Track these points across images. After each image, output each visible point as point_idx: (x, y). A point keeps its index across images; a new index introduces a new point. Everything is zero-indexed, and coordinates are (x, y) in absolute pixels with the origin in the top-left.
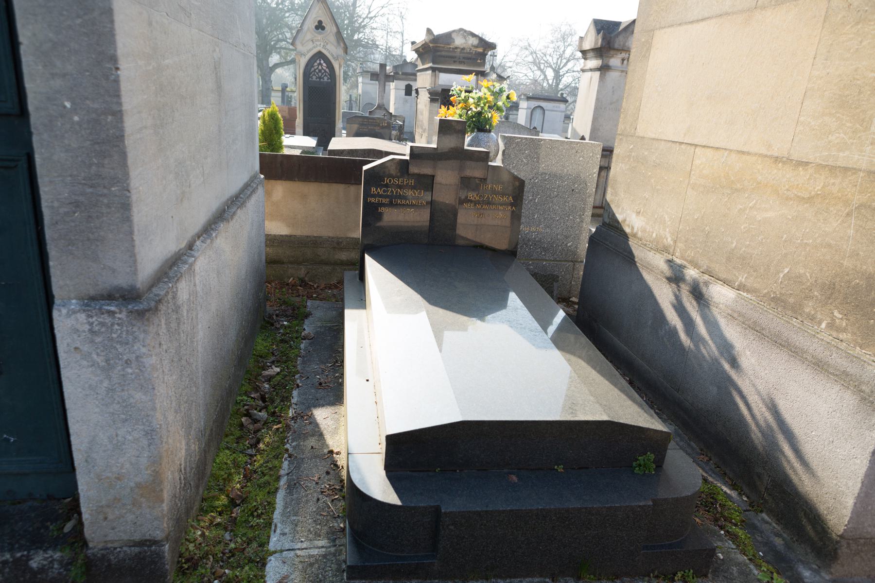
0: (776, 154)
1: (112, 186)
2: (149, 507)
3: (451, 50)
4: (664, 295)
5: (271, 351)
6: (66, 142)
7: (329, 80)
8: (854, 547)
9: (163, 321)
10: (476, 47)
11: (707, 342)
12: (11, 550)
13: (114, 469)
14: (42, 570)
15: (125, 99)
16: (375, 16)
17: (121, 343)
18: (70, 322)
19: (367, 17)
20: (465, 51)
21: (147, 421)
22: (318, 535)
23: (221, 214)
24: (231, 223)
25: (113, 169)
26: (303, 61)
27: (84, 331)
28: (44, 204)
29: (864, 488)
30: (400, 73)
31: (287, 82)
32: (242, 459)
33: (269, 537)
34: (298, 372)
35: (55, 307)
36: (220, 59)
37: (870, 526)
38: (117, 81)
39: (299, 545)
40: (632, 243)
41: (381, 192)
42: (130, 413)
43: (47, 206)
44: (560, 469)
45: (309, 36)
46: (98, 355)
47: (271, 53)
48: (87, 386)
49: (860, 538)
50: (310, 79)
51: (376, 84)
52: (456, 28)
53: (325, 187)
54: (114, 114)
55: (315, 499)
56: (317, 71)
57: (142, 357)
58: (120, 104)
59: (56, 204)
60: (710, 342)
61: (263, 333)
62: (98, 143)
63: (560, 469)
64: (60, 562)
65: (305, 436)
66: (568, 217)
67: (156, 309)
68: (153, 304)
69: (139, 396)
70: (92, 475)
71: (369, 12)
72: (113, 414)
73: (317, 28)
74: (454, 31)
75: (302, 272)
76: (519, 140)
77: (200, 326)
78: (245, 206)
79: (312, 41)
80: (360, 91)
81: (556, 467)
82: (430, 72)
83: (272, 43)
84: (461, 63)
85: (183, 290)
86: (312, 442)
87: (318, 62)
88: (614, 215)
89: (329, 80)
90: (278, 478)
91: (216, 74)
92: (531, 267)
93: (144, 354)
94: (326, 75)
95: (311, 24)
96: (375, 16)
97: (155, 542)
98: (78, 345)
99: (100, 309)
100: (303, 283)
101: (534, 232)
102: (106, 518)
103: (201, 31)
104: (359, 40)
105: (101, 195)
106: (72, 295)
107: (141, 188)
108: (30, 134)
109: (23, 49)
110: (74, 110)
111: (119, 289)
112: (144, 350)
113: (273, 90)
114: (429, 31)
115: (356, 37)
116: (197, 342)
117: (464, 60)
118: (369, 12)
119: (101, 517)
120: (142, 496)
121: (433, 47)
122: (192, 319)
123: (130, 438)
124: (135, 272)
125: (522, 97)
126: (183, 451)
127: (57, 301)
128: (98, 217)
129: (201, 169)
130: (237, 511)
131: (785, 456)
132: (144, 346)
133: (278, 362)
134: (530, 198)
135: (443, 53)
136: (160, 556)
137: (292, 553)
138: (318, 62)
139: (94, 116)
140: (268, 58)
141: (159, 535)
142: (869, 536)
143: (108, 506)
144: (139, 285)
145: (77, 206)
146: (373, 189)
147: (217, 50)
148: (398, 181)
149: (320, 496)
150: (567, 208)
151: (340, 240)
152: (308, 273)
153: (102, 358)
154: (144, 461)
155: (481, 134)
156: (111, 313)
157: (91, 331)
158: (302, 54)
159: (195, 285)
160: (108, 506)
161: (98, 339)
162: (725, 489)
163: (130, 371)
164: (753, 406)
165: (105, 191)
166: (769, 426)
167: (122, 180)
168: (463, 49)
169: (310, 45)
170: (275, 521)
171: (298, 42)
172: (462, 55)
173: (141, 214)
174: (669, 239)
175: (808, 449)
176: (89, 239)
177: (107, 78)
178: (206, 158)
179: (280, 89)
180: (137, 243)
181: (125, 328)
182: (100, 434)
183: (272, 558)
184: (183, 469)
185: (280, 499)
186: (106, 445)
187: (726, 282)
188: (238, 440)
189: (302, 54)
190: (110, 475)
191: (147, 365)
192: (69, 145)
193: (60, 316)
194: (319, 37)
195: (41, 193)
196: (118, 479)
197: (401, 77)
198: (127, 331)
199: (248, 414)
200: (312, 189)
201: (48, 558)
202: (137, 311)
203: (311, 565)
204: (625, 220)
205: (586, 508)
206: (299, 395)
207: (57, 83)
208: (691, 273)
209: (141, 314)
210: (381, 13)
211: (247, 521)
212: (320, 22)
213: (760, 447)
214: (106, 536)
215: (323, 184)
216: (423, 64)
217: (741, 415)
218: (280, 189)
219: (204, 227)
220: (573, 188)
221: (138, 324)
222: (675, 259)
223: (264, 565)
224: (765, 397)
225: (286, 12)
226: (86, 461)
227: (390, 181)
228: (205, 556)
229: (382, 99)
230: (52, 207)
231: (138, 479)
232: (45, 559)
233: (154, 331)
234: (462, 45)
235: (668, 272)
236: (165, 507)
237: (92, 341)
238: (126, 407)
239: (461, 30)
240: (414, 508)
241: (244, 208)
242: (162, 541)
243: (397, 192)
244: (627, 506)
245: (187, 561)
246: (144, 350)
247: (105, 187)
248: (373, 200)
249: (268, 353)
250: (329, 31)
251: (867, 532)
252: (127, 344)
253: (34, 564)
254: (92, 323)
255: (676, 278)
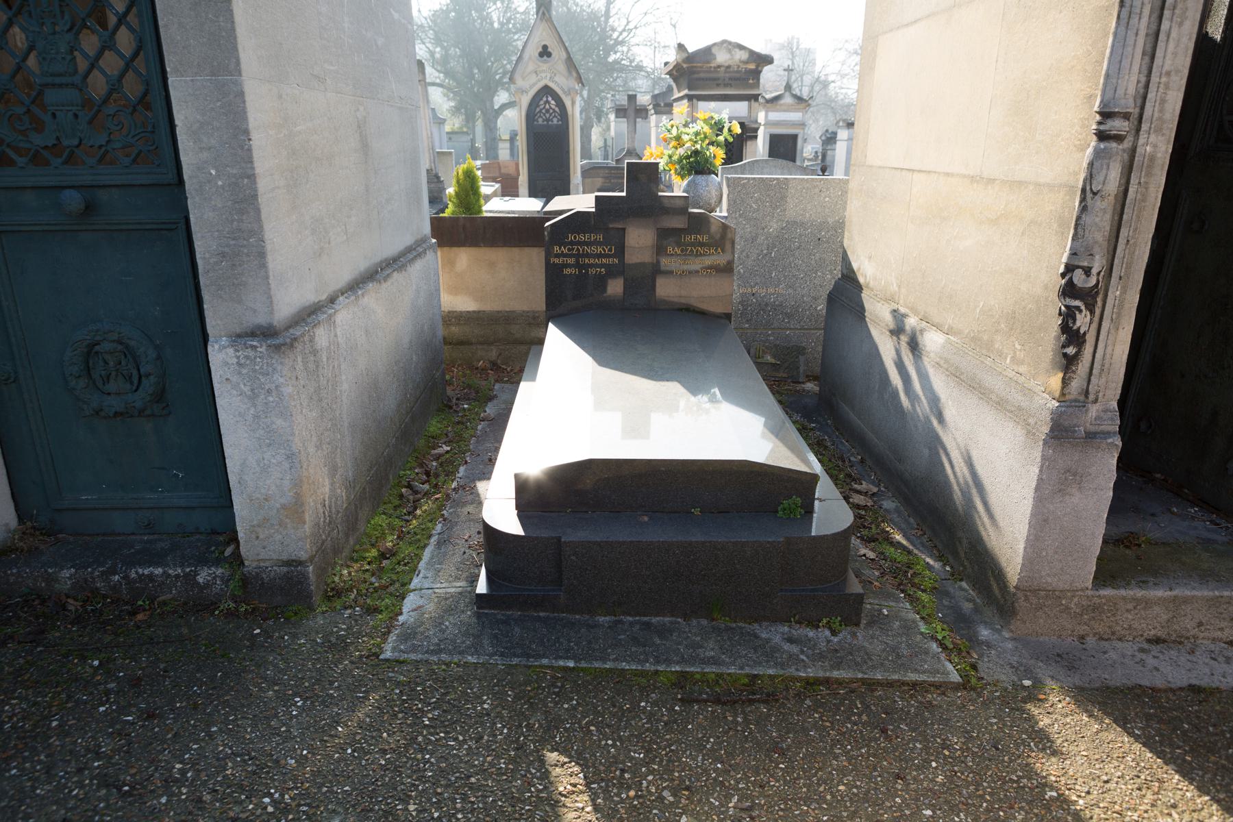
0: (972, 174)
1: (250, 238)
2: (294, 528)
3: (712, 69)
4: (887, 348)
5: (445, 432)
6: (213, 203)
7: (560, 123)
8: (1034, 600)
9: (299, 359)
10: (746, 62)
11: (920, 398)
12: (182, 566)
13: (263, 491)
14: (207, 585)
15: (257, 164)
16: (636, 28)
17: (263, 374)
18: (221, 356)
19: (624, 30)
20: (731, 70)
21: (288, 445)
22: (457, 578)
23: (372, 276)
24: (384, 285)
25: (250, 223)
26: (525, 100)
27: (233, 364)
28: (198, 256)
29: (1032, 530)
30: (662, 105)
31: (516, 129)
32: (397, 522)
33: (411, 579)
34: (469, 450)
35: (209, 343)
36: (365, 117)
37: (1048, 575)
38: (250, 150)
39: (438, 585)
40: (865, 295)
41: (566, 251)
42: (273, 438)
43: (201, 258)
44: (697, 511)
45: (531, 67)
46: (245, 385)
47: (496, 91)
48: (237, 413)
49: (1039, 590)
50: (535, 123)
51: (624, 122)
52: (718, 39)
53: (516, 251)
54: (249, 177)
55: (462, 553)
56: (544, 111)
57: (280, 387)
58: (253, 168)
59: (207, 255)
60: (923, 398)
61: (439, 415)
62: (238, 202)
63: (697, 511)
64: (222, 579)
65: (465, 504)
66: (816, 273)
67: (292, 346)
68: (288, 340)
69: (279, 422)
70: (244, 496)
71: (628, 22)
72: (259, 439)
73: (541, 55)
74: (715, 44)
75: (493, 354)
76: (745, 181)
77: (344, 377)
78: (405, 270)
79: (536, 72)
80: (612, 133)
81: (693, 510)
82: (685, 101)
83: (497, 77)
84: (726, 86)
85: (322, 336)
86: (470, 508)
87: (545, 99)
88: (850, 263)
89: (560, 123)
90: (430, 536)
91: (360, 133)
92: (771, 338)
93: (282, 383)
94: (555, 116)
95: (533, 50)
96: (636, 28)
97: (300, 563)
98: (228, 377)
99: (245, 344)
100: (495, 366)
101: (773, 294)
102: (258, 537)
103: (339, 93)
104: (616, 62)
105: (242, 246)
106: (223, 333)
107: (275, 240)
108: (186, 198)
109: (178, 130)
110: (218, 176)
111: (259, 327)
112: (282, 380)
113: (501, 140)
114: (681, 47)
115: (611, 59)
116: (341, 391)
117: (730, 82)
118: (628, 22)
119: (254, 536)
120: (287, 517)
121: (688, 68)
122: (334, 367)
123: (274, 461)
124: (272, 312)
125: (841, 124)
126: (327, 489)
127: (211, 339)
128: (240, 265)
129: (343, 227)
130: (385, 563)
131: (978, 512)
132: (281, 377)
133: (449, 442)
134: (765, 252)
135: (702, 75)
136: (305, 576)
137: (431, 591)
138: (545, 99)
139: (233, 180)
140: (493, 97)
141: (303, 556)
142: (1050, 588)
143: (259, 526)
144: (275, 324)
145: (224, 256)
146: (556, 248)
147: (361, 108)
148: (585, 237)
149: (467, 551)
150: (813, 262)
151: (537, 315)
152: (500, 354)
153: (248, 388)
154: (287, 483)
155: (700, 178)
156: (254, 348)
157: (239, 364)
158: (523, 91)
159: (336, 336)
160: (259, 526)
161: (244, 371)
162: (928, 560)
163: (271, 399)
164: (955, 461)
165: (245, 242)
166: (966, 483)
167: (257, 232)
168: (729, 67)
169: (533, 78)
170: (420, 568)
171: (517, 77)
172: (727, 75)
173: (275, 262)
174: (895, 285)
175: (993, 499)
176: (233, 284)
177: (242, 148)
178: (349, 217)
179: (507, 137)
180: (273, 286)
181: (265, 361)
182: (250, 457)
183: (412, 594)
184: (327, 505)
185: (427, 554)
186: (255, 468)
187: (938, 327)
188: (396, 508)
189: (523, 91)
190: (259, 496)
191: (285, 394)
192: (216, 206)
193: (213, 351)
194: (545, 67)
195: (196, 246)
196: (266, 500)
197: (663, 109)
198: (267, 363)
199: (409, 486)
200: (499, 255)
201: (211, 574)
202: (274, 345)
203: (446, 599)
204: (859, 269)
205: (710, 542)
206: (465, 470)
207: (205, 155)
208: (911, 322)
209: (278, 348)
210: (643, 22)
211: (393, 569)
212: (545, 47)
213: (960, 508)
214: (258, 555)
215: (514, 249)
216: (679, 91)
217: (946, 476)
218: (464, 257)
219: (349, 284)
220: (819, 237)
221: (276, 357)
222: (900, 308)
223: (403, 598)
224: (963, 450)
225: (515, 33)
226: (239, 482)
227: (575, 237)
228: (350, 590)
229: (633, 142)
230: (205, 258)
231: (283, 501)
232: (209, 575)
233: (291, 364)
234: (725, 62)
235: (892, 326)
236: (307, 528)
237: (240, 373)
238: (269, 432)
239: (724, 42)
240: (537, 538)
241: (403, 272)
242: (306, 561)
243: (583, 250)
244: (755, 542)
245: (333, 589)
246: (282, 380)
247: (244, 239)
248: (556, 261)
249: (441, 434)
250: (557, 57)
251: (1046, 583)
252: (268, 375)
253: (200, 579)
254: (239, 356)
255: (897, 331)
